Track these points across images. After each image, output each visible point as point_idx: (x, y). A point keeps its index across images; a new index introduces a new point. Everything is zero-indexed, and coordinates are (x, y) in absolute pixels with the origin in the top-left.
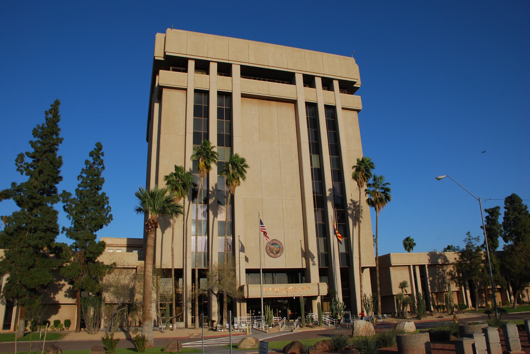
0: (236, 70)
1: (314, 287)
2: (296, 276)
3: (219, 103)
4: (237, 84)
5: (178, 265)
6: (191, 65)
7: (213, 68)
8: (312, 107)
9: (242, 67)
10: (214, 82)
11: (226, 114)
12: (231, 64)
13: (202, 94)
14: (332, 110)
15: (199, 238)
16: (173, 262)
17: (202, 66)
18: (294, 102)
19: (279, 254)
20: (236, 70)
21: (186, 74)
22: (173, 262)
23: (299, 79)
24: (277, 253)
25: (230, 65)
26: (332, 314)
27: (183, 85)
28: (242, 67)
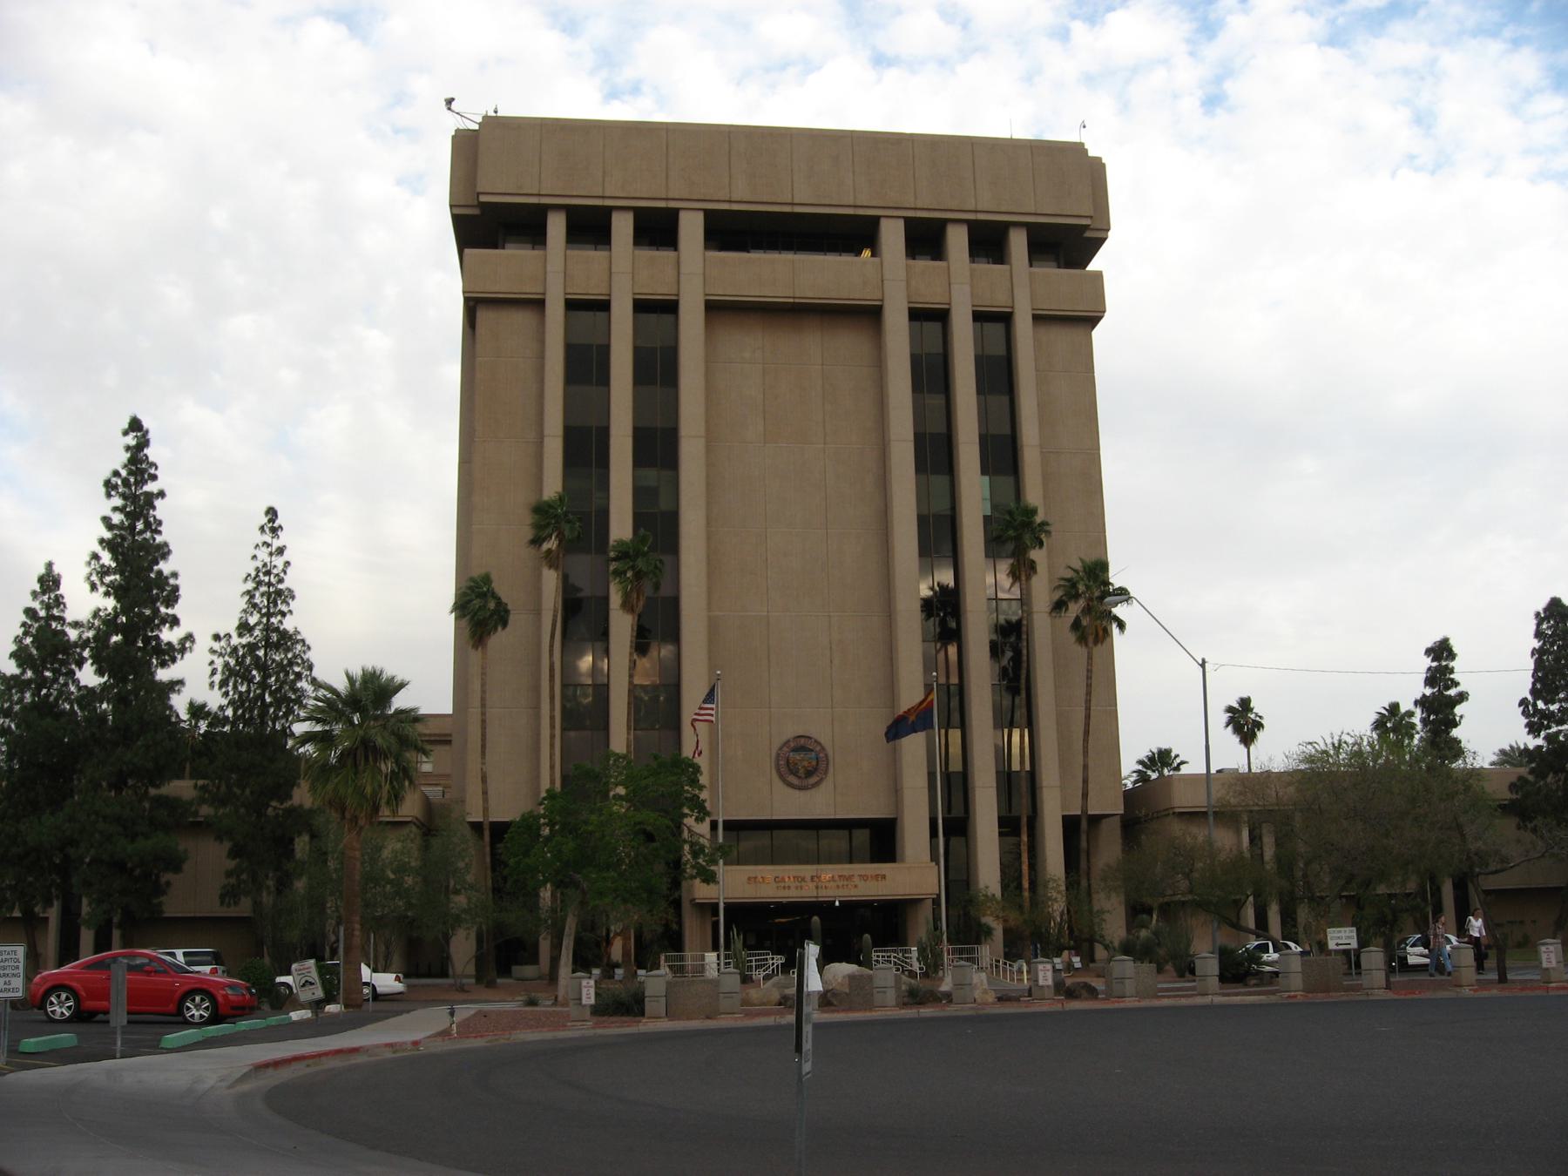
0: (691, 228)
1: (914, 874)
2: (881, 840)
3: (980, 340)
4: (695, 270)
5: (873, 809)
6: (556, 226)
7: (622, 227)
8: (929, 317)
9: (909, 222)
10: (624, 270)
11: (658, 368)
12: (676, 212)
13: (929, 317)
14: (937, 326)
15: (951, 731)
16: (1085, 795)
17: (589, 227)
18: (870, 315)
19: (813, 780)
20: (691, 228)
21: (666, 255)
22: (1085, 795)
23: (892, 236)
24: (809, 774)
25: (874, 222)
26: (1069, 948)
27: (529, 289)
28: (909, 222)
